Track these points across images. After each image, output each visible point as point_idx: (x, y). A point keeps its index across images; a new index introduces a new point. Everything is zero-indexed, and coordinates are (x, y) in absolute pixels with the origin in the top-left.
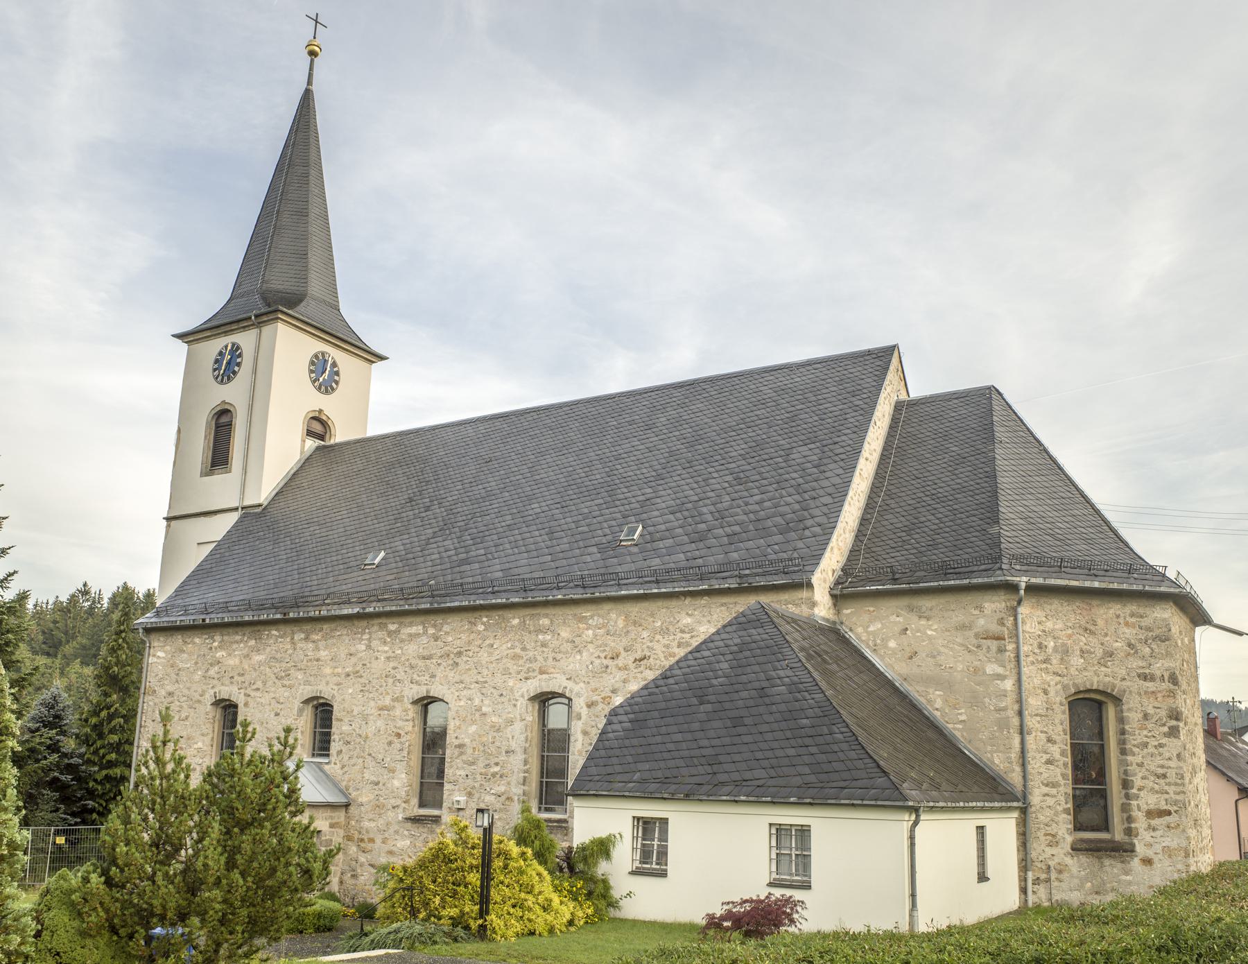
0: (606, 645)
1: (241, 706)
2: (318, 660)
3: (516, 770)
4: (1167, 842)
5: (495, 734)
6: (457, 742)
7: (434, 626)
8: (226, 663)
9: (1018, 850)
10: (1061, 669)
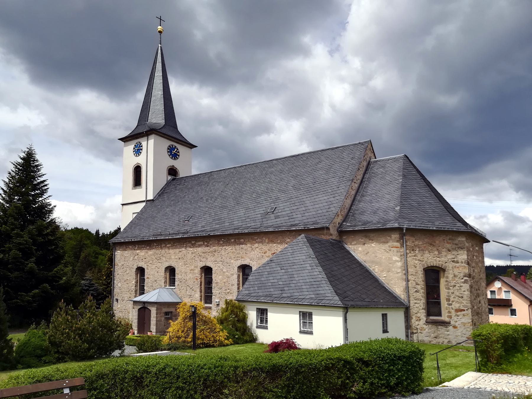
0: (262, 248)
1: (146, 269)
2: (170, 254)
3: (235, 291)
4: (463, 320)
5: (228, 279)
6: (215, 282)
7: (207, 242)
8: (140, 255)
9: (405, 322)
10: (421, 258)
